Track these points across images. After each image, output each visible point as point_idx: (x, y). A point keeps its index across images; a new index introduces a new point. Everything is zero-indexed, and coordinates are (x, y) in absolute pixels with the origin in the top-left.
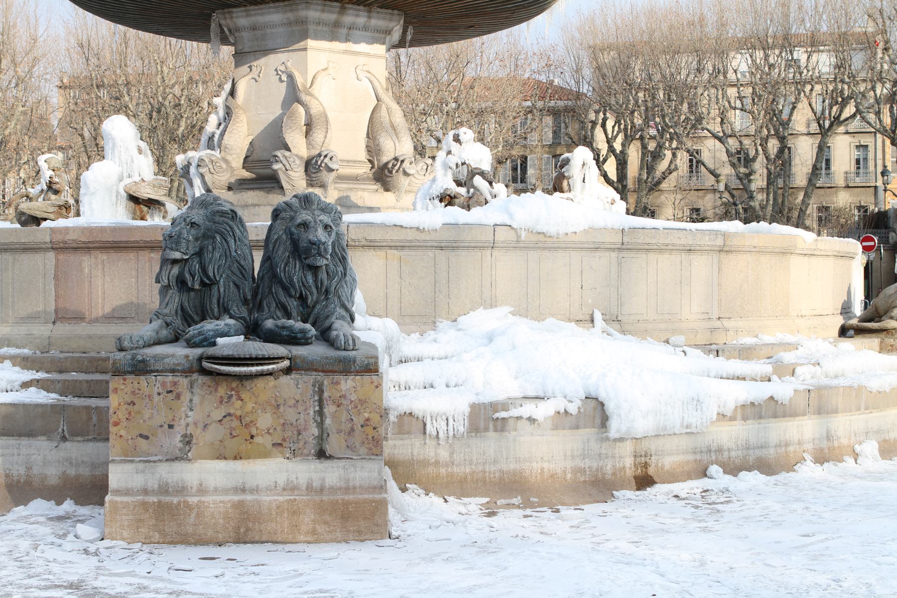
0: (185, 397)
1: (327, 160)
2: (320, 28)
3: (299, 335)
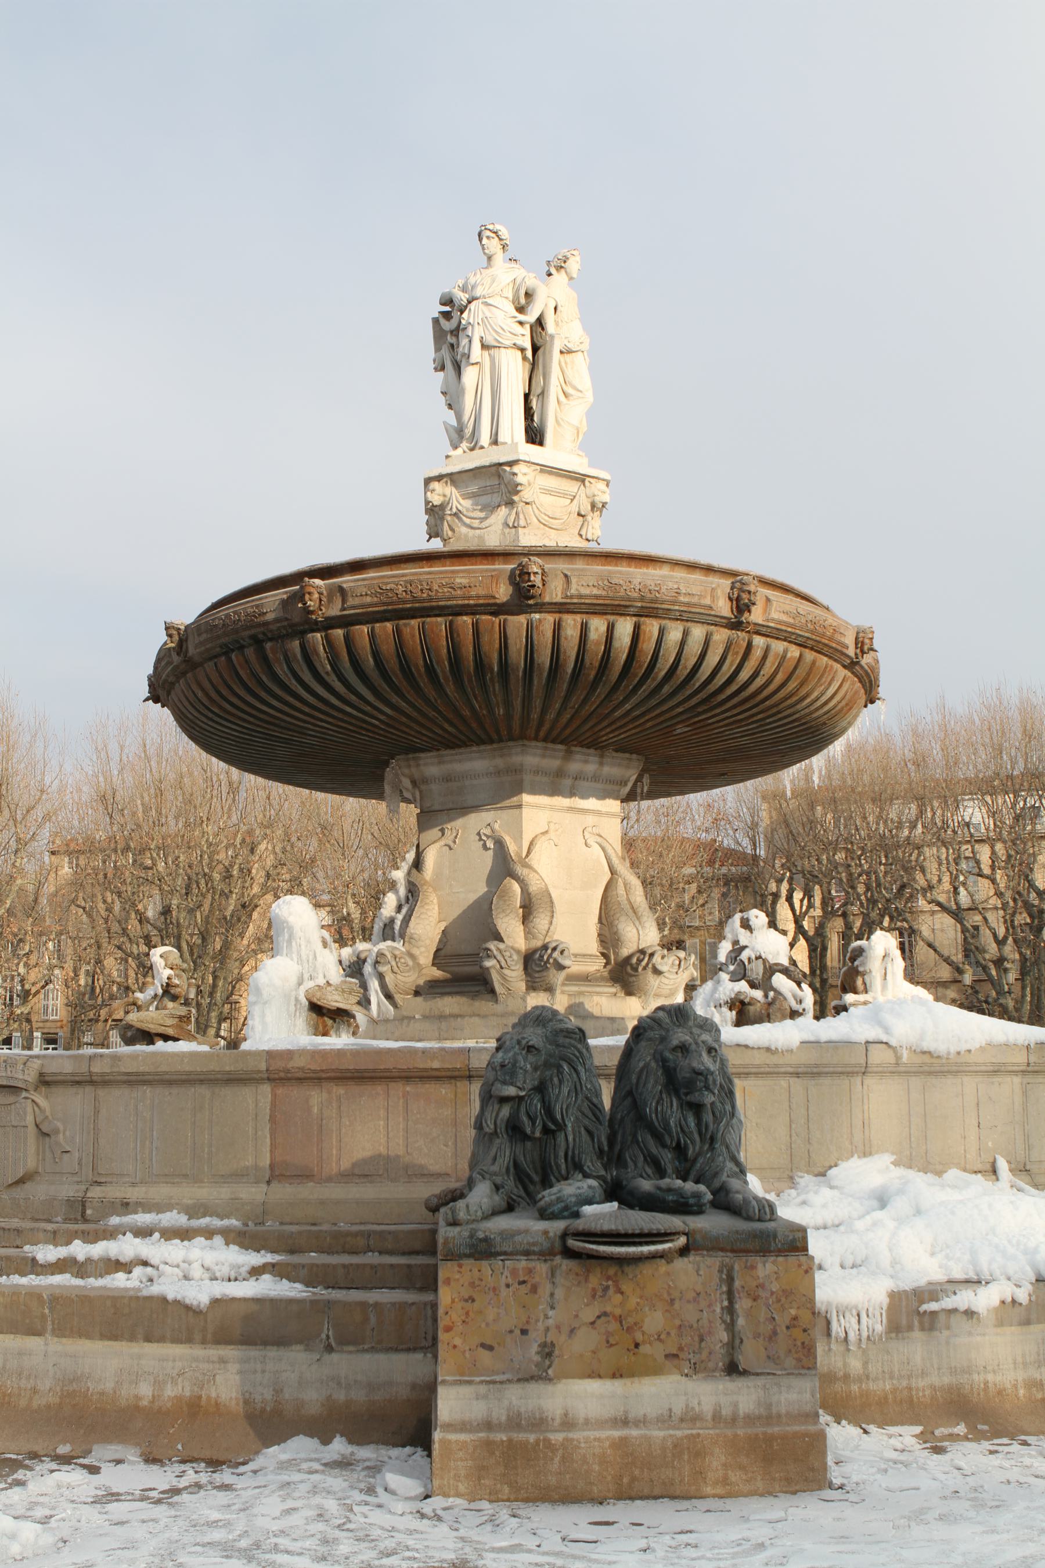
0: (545, 1289)
1: (556, 954)
2: (538, 778)
3: (691, 1201)
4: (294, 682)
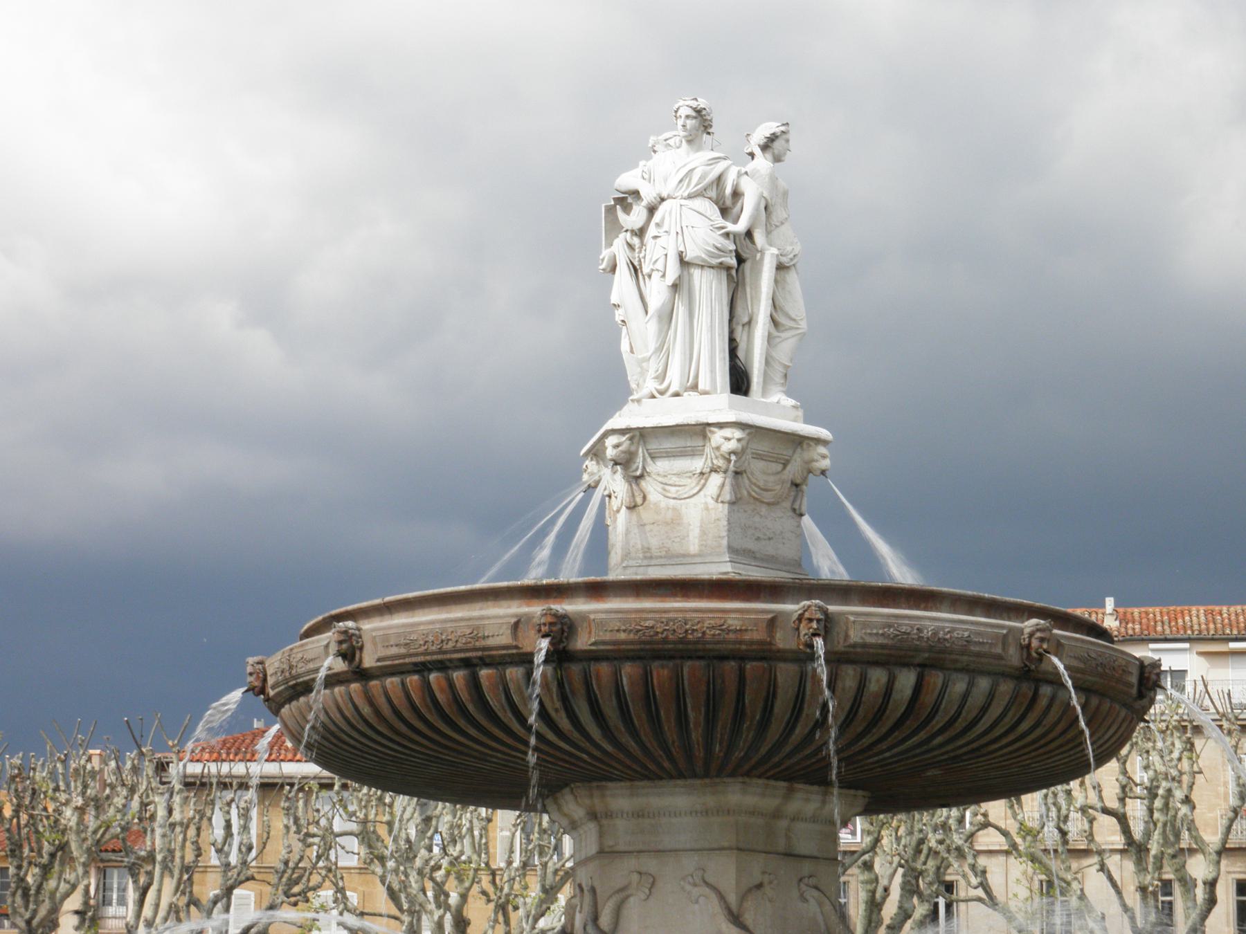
4: (510, 715)
